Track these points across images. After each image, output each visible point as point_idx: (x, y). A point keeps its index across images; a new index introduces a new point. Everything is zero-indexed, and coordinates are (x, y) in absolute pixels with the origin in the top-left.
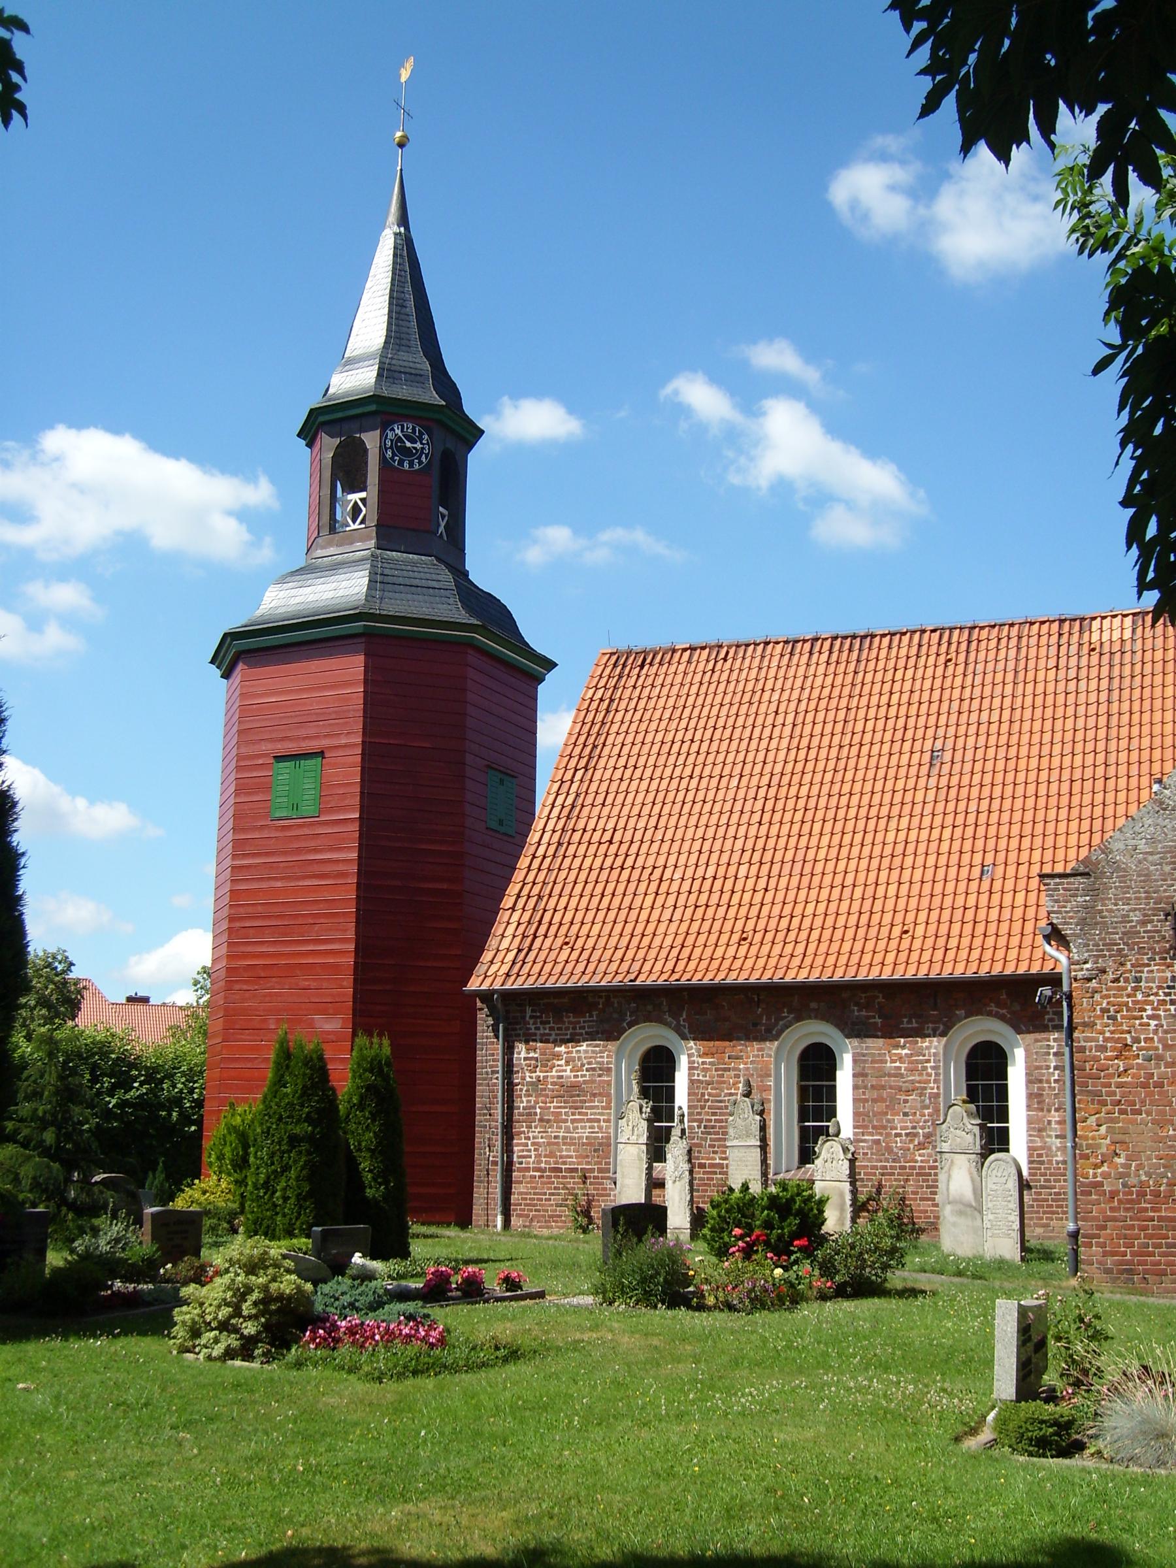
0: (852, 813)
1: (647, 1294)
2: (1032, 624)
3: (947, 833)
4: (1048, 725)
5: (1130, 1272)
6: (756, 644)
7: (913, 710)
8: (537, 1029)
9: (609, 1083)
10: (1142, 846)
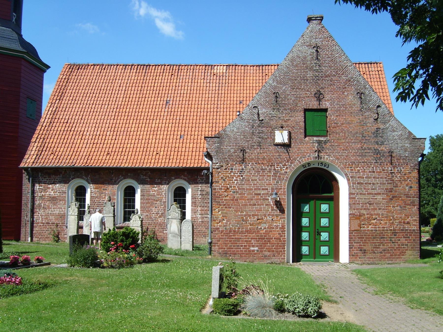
0: (142, 118)
1: (86, 263)
2: (197, 66)
3: (170, 125)
4: (201, 95)
5: (226, 253)
6: (114, 65)
7: (161, 88)
8: (42, 179)
9: (65, 197)
10: (235, 130)
